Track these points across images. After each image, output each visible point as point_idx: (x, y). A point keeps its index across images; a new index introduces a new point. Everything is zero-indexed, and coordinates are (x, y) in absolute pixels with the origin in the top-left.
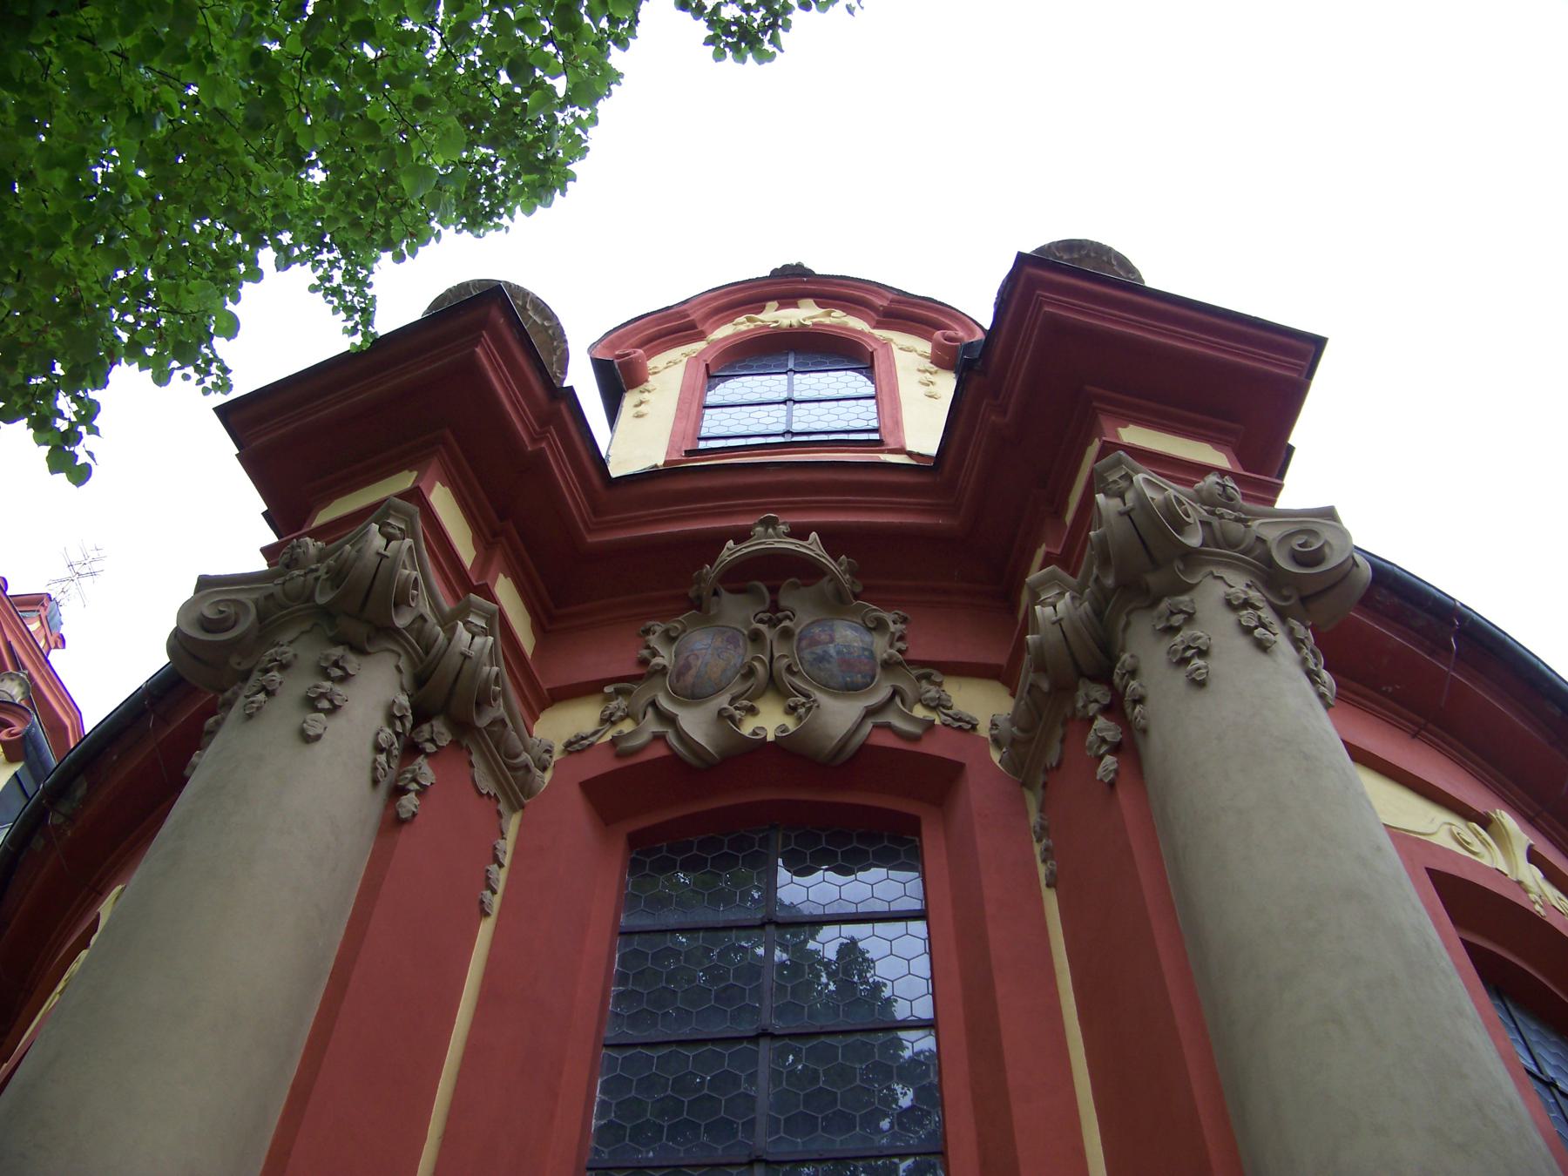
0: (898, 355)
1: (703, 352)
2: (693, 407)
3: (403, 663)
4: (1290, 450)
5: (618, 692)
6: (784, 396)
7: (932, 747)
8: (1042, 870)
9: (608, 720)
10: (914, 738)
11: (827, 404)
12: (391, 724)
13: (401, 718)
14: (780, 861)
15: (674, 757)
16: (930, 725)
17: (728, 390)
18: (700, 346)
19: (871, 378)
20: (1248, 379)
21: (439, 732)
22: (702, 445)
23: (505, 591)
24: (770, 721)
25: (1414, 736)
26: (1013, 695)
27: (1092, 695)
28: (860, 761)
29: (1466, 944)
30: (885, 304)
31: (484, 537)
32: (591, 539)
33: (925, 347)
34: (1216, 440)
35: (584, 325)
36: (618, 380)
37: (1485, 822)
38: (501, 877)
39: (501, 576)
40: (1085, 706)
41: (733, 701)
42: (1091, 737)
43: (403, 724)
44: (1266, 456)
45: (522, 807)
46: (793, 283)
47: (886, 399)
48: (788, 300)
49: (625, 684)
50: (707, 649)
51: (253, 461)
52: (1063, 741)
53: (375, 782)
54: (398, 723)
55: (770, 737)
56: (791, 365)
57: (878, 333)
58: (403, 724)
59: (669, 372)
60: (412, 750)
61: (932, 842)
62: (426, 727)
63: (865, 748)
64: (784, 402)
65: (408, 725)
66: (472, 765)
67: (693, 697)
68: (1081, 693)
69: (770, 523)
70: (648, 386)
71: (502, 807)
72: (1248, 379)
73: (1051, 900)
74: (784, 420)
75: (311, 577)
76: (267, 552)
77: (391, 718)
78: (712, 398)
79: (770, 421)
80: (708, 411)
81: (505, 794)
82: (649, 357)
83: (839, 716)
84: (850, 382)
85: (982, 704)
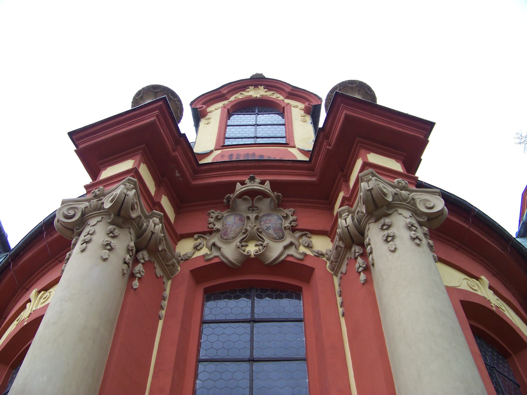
0: (293, 109)
1: (228, 105)
2: (224, 126)
3: (132, 231)
4: (421, 159)
5: (199, 237)
6: (254, 123)
7: (307, 263)
8: (339, 300)
9: (197, 248)
10: (302, 260)
11: (267, 125)
12: (128, 253)
13: (132, 250)
14: (177, 171)
15: (222, 262)
16: (305, 255)
17: (236, 119)
18: (226, 102)
19: (283, 118)
20: (408, 137)
21: (144, 255)
22: (228, 142)
23: (165, 202)
24: (252, 249)
25: (457, 250)
26: (332, 241)
27: (357, 249)
28: (283, 266)
29: (471, 325)
30: (289, 90)
31: (158, 184)
32: (194, 183)
33: (301, 106)
34: (397, 159)
35: (187, 97)
36: (199, 116)
37: (477, 279)
38: (165, 303)
39: (163, 195)
40: (358, 268)
41: (240, 242)
42: (357, 265)
43: (132, 252)
44: (412, 162)
45: (171, 278)
46: (258, 80)
47: (288, 125)
48: (256, 86)
49: (203, 234)
50: (231, 222)
51: (81, 153)
52: (347, 265)
53: (124, 274)
54: (131, 252)
55: (253, 256)
56: (257, 112)
57: (287, 101)
58: (132, 252)
59: (216, 112)
60: (136, 261)
61: (305, 293)
62: (141, 252)
63: (284, 261)
64: (254, 125)
65: (134, 252)
66: (155, 268)
67: (227, 241)
68: (353, 249)
69: (252, 179)
70: (208, 117)
71: (165, 280)
72: (408, 137)
73: (343, 320)
74: (254, 132)
75: (100, 202)
76: (87, 187)
77: (129, 250)
78: (230, 122)
79: (250, 131)
80: (228, 127)
81: (166, 275)
82: (208, 107)
83: (275, 250)
84: (275, 118)
85: (322, 244)
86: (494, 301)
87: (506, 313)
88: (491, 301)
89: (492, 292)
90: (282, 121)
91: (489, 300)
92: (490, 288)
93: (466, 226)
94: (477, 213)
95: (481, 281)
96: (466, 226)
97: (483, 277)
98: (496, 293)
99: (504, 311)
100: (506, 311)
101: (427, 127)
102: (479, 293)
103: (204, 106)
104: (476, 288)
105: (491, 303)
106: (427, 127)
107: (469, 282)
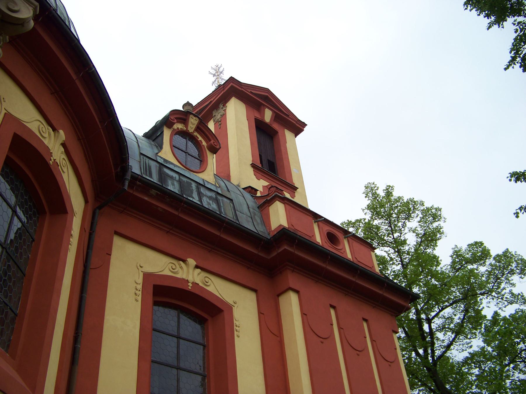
25: (51, 94)
82: (178, 122)
86: (58, 155)
87: (65, 176)
88: (53, 155)
89: (63, 149)
90: (199, 338)
91: (51, 153)
92: (63, 145)
93: (74, 77)
94: (93, 72)
95: (57, 134)
96: (74, 77)
97: (61, 132)
98: (67, 152)
99: (64, 172)
100: (66, 173)
101: (304, 125)
102: (46, 142)
103: (175, 121)
104: (46, 135)
105: (52, 156)
106: (304, 125)
107: (42, 126)
